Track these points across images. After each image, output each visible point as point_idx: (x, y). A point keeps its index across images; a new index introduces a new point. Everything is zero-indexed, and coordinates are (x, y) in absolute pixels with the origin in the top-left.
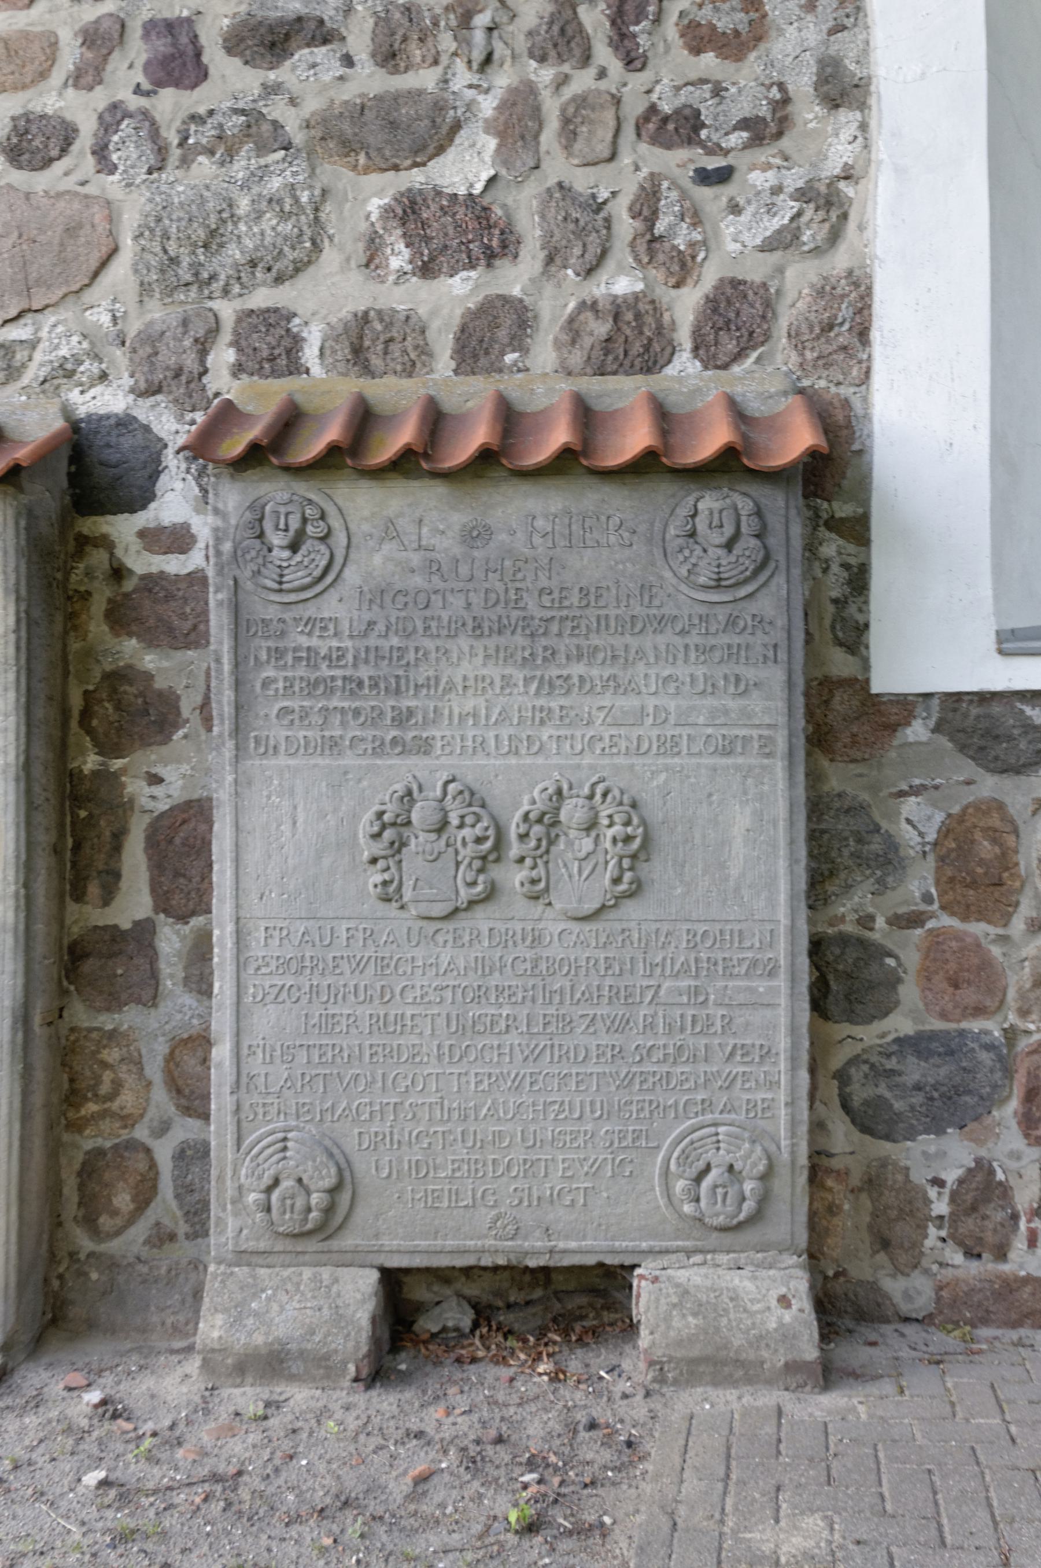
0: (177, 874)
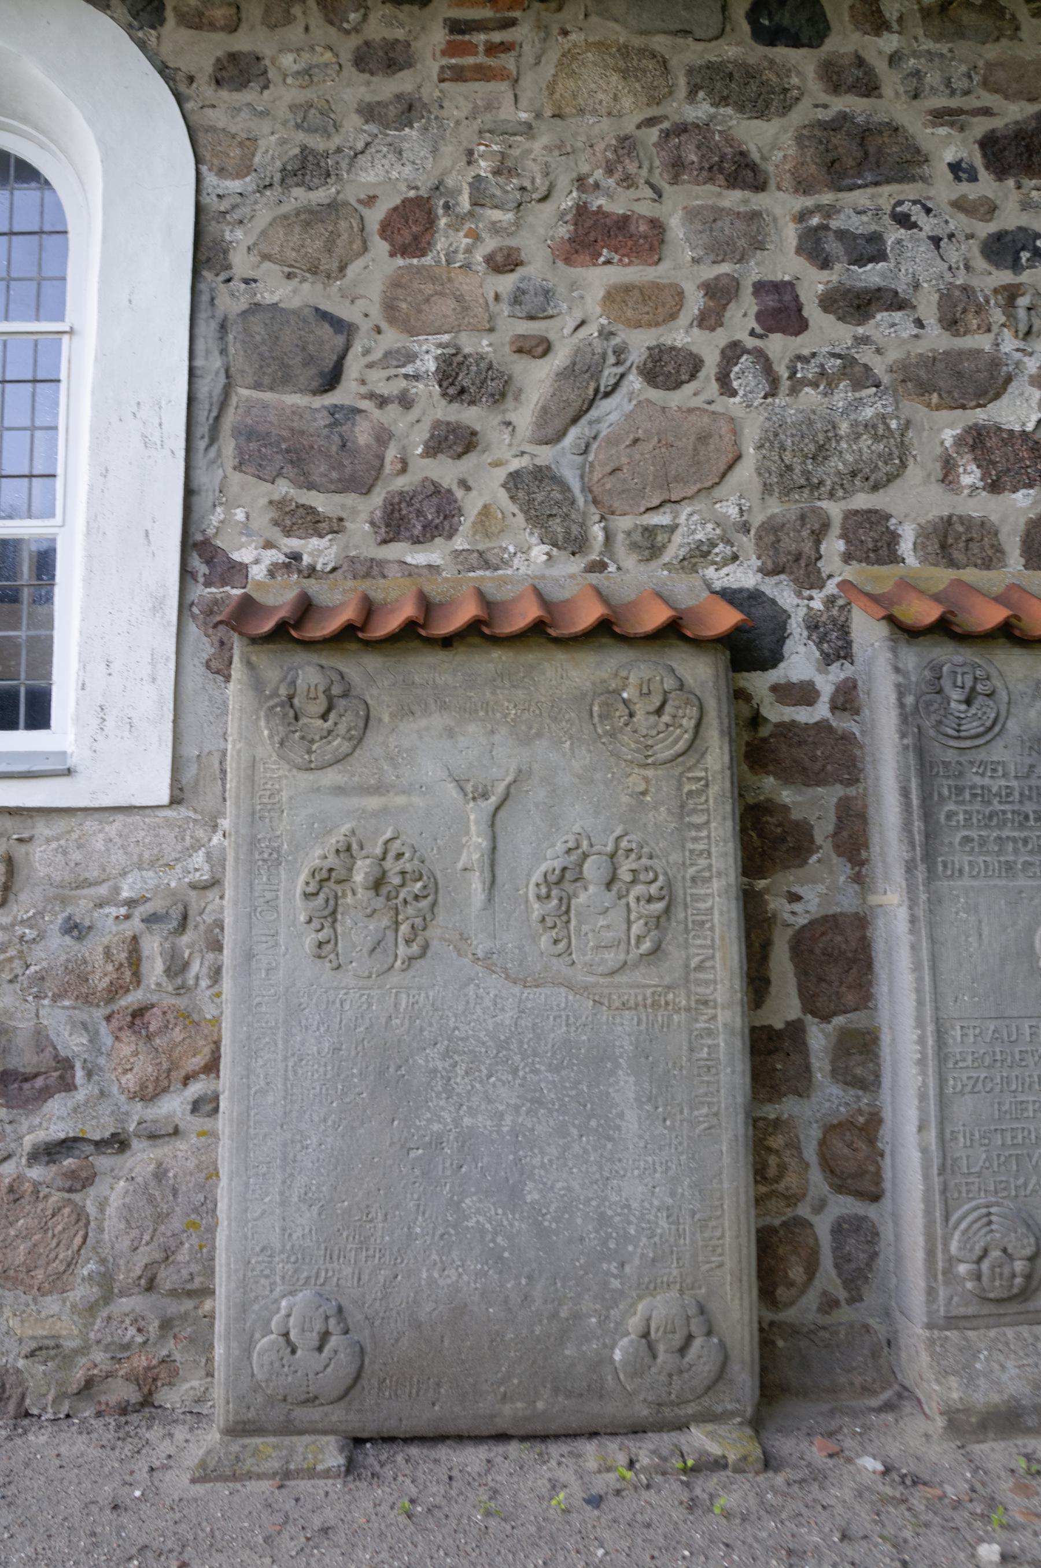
0: (821, 980)
